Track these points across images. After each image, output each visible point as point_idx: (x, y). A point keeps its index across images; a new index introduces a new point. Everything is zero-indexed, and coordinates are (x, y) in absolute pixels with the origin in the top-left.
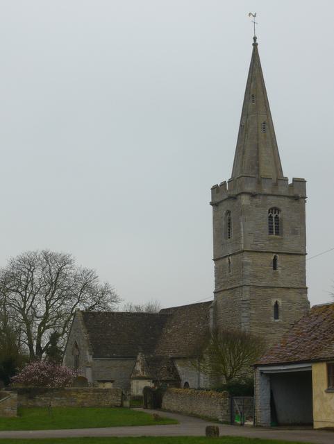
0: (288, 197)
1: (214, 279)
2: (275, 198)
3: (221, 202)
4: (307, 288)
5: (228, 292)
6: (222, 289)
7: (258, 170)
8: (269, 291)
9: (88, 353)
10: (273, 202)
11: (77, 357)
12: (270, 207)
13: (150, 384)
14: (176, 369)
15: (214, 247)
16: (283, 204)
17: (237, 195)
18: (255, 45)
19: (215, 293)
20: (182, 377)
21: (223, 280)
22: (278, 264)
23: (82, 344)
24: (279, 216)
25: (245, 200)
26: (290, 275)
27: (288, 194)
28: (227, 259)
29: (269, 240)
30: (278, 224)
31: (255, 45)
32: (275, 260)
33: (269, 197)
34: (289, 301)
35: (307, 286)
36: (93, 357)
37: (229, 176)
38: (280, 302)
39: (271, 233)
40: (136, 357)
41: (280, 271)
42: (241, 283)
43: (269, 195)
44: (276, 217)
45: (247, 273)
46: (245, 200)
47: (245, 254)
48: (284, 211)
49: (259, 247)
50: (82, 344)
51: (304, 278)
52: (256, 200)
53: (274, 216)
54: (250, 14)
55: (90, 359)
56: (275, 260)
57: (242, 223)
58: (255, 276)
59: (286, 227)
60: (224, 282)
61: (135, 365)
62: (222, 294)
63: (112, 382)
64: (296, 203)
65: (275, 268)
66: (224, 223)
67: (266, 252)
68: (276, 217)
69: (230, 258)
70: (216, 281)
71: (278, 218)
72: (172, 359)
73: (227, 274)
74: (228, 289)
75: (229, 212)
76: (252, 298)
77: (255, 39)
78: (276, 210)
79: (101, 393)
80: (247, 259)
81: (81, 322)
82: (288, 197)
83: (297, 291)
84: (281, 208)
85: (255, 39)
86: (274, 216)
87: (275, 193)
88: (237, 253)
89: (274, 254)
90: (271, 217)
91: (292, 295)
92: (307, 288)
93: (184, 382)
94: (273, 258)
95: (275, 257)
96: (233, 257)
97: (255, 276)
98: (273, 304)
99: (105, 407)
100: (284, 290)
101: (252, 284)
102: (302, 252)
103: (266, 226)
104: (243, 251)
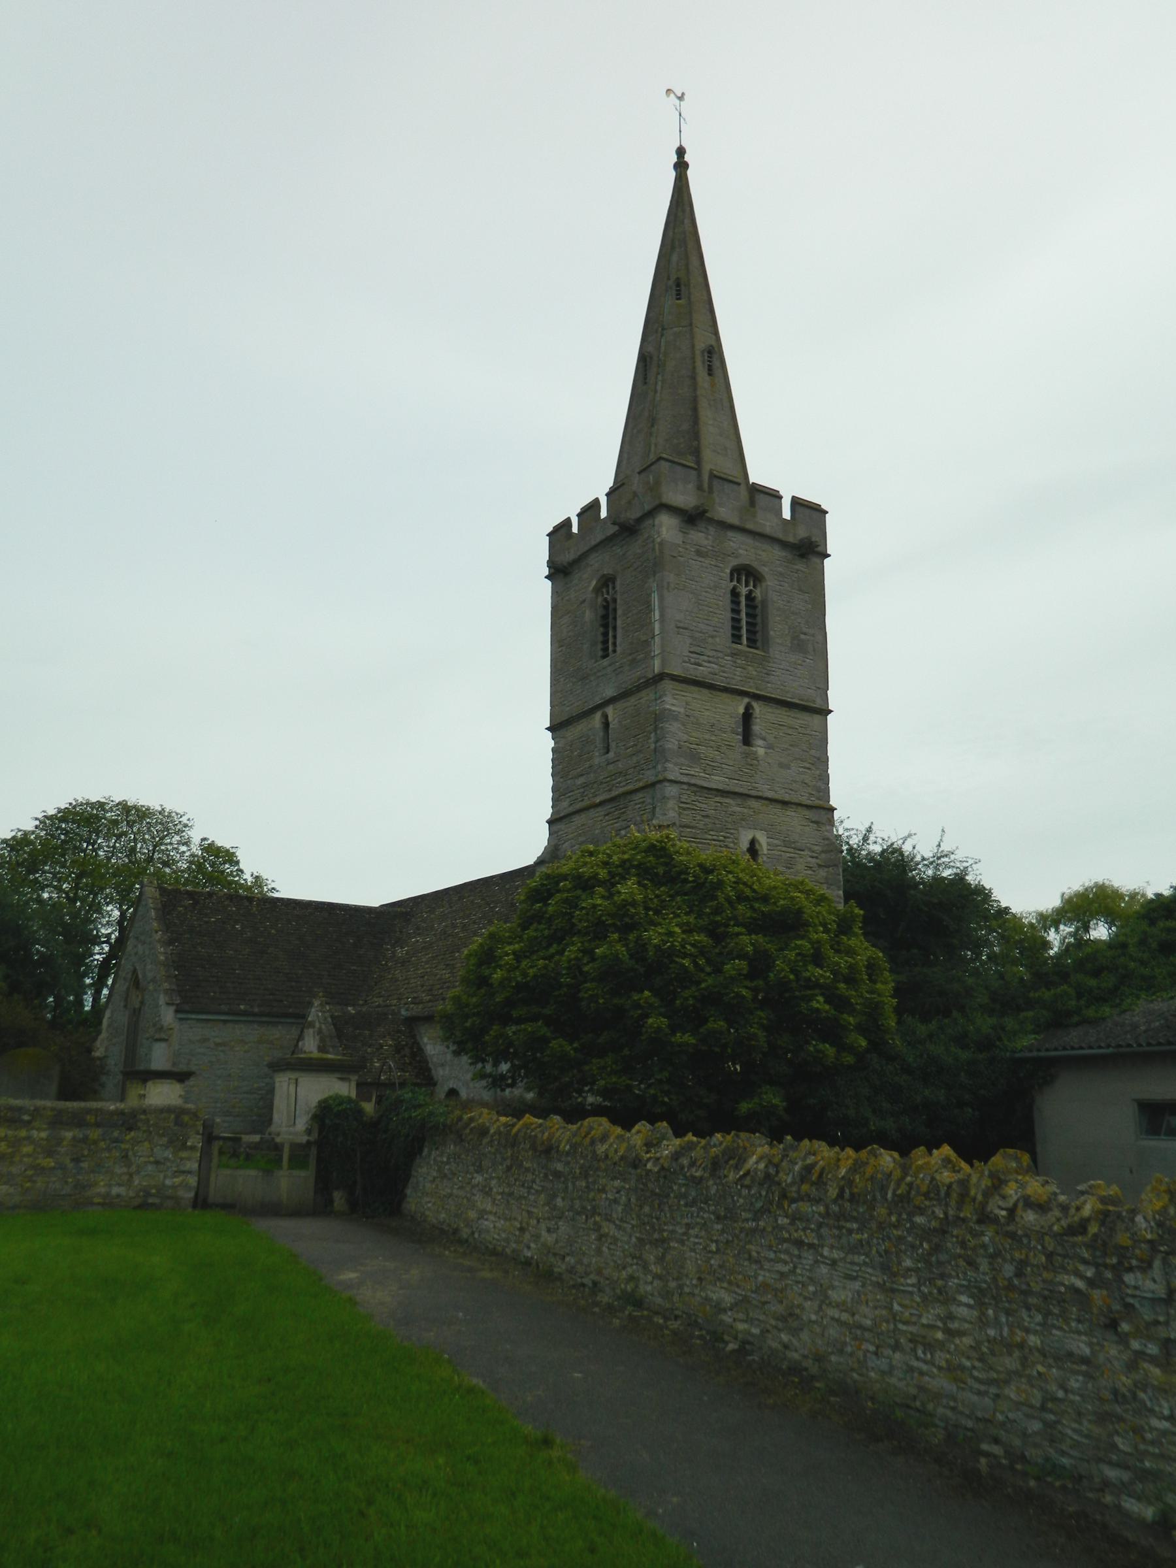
0: (784, 544)
1: (551, 794)
2: (749, 540)
3: (584, 556)
4: (833, 809)
5: (601, 811)
6: (579, 806)
7: (697, 453)
8: (733, 805)
9: (162, 999)
10: (744, 550)
11: (136, 1013)
12: (734, 562)
13: (343, 1088)
14: (421, 1050)
15: (456, 886)
16: (768, 559)
17: (640, 520)
18: (681, 166)
19: (550, 822)
20: (439, 1073)
21: (580, 781)
22: (756, 728)
23: (150, 975)
24: (758, 593)
25: (667, 527)
26: (788, 767)
27: (780, 536)
28: (598, 716)
29: (733, 655)
30: (754, 616)
31: (681, 166)
32: (747, 717)
33: (730, 534)
34: (787, 844)
35: (833, 803)
36: (177, 1011)
37: (609, 482)
38: (762, 838)
39: (736, 638)
40: (304, 1017)
41: (761, 751)
42: (650, 776)
43: (732, 527)
44: (750, 597)
45: (671, 744)
46: (667, 527)
47: (667, 685)
48: (770, 582)
49: (702, 672)
50: (150, 975)
51: (825, 778)
52: (699, 537)
53: (744, 591)
54: (669, 91)
55: (168, 1016)
56: (747, 717)
57: (655, 598)
58: (694, 757)
59: (777, 628)
60: (585, 786)
61: (301, 1037)
62: (578, 820)
63: (181, 1077)
64: (800, 566)
65: (747, 740)
66: (589, 615)
67: (726, 690)
68: (750, 597)
69: (610, 710)
70: (554, 789)
71: (753, 599)
72: (412, 1021)
73: (596, 761)
74: (601, 803)
75: (607, 581)
76: (685, 821)
77: (681, 152)
78: (746, 573)
79: (95, 1134)
80: (673, 700)
81: (153, 913)
82: (784, 544)
83: (807, 813)
84: (764, 570)
85: (681, 152)
86: (744, 591)
87: (749, 526)
88: (638, 689)
89: (746, 700)
90: (735, 594)
91: (794, 822)
92: (833, 809)
93: (446, 1089)
94: (741, 710)
95: (748, 708)
96: (620, 705)
97: (694, 757)
98: (745, 845)
99: (109, 1203)
100: (776, 810)
101: (685, 779)
102: (818, 704)
103: (724, 616)
104: (661, 677)
